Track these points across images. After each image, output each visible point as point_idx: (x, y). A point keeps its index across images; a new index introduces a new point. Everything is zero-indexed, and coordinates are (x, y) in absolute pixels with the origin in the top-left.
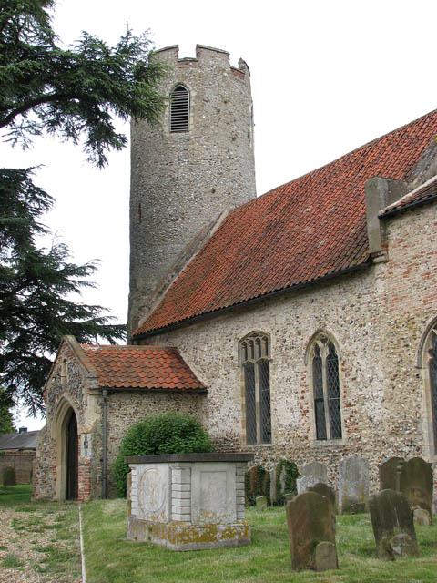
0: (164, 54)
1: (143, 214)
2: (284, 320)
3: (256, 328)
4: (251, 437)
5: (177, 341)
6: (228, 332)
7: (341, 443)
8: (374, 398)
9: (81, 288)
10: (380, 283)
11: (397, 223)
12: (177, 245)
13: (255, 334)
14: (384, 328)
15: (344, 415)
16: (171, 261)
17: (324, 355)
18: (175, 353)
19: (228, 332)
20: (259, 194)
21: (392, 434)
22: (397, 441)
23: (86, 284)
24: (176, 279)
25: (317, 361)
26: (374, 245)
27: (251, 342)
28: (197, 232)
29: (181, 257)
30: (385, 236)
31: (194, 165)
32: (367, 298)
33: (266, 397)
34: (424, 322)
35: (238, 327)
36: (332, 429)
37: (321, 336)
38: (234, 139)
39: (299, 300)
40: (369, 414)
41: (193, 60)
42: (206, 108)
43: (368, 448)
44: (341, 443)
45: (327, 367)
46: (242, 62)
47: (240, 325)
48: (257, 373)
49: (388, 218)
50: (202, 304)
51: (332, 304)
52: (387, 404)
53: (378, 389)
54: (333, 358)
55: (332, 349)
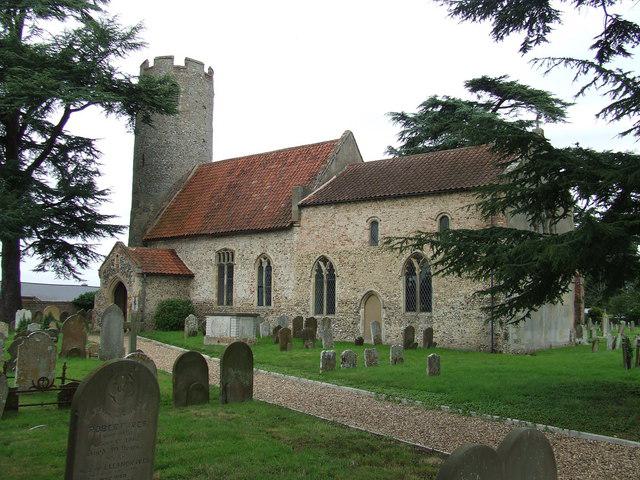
4: (260, 303)
5: (174, 246)
7: (270, 308)
10: (296, 236)
12: (168, 184)
13: (226, 249)
14: (295, 257)
15: (273, 295)
16: (163, 193)
17: (265, 265)
18: (173, 252)
20: (215, 159)
22: (298, 309)
25: (261, 268)
26: (294, 218)
30: (300, 214)
31: (180, 135)
32: (288, 242)
33: (230, 283)
37: (264, 256)
41: (183, 68)
44: (270, 308)
45: (265, 271)
46: (210, 69)
48: (226, 270)
49: (302, 207)
50: (193, 227)
53: (291, 285)
54: (269, 268)
55: (269, 263)
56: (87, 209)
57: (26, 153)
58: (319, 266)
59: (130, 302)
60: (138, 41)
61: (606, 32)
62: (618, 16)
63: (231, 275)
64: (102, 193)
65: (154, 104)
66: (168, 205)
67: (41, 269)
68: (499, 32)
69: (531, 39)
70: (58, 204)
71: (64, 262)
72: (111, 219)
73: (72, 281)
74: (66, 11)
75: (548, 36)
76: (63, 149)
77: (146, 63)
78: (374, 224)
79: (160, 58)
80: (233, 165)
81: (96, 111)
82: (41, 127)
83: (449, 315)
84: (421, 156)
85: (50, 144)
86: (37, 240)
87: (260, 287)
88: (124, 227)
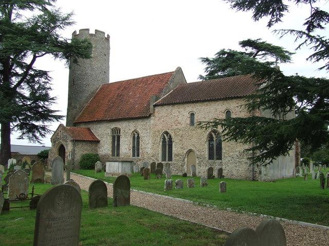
4: (134, 155)
5: (89, 126)
7: (139, 158)
10: (152, 121)
13: (116, 128)
14: (152, 132)
15: (140, 151)
16: (84, 99)
17: (136, 136)
18: (89, 129)
20: (110, 82)
25: (134, 137)
26: (151, 112)
29: (88, 98)
30: (154, 110)
31: (92, 69)
32: (148, 124)
33: (118, 145)
37: (135, 131)
44: (139, 158)
45: (136, 139)
46: (108, 35)
48: (116, 138)
49: (155, 106)
50: (99, 116)
53: (150, 146)
54: (138, 137)
55: (138, 135)
56: (45, 107)
57: (14, 79)
58: (164, 136)
59: (67, 154)
60: (71, 21)
61: (311, 16)
62: (317, 8)
63: (119, 141)
64: (52, 99)
65: (79, 54)
66: (86, 105)
67: (21, 138)
68: (256, 16)
69: (273, 20)
70: (30, 105)
71: (33, 134)
73: (37, 144)
74: (34, 6)
75: (282, 19)
76: (32, 76)
77: (75, 32)
78: (192, 115)
79: (82, 30)
80: (120, 85)
81: (49, 57)
82: (21, 65)
83: (231, 161)
84: (216, 80)
85: (26, 74)
86: (19, 123)
87: (134, 147)
88: (64, 116)
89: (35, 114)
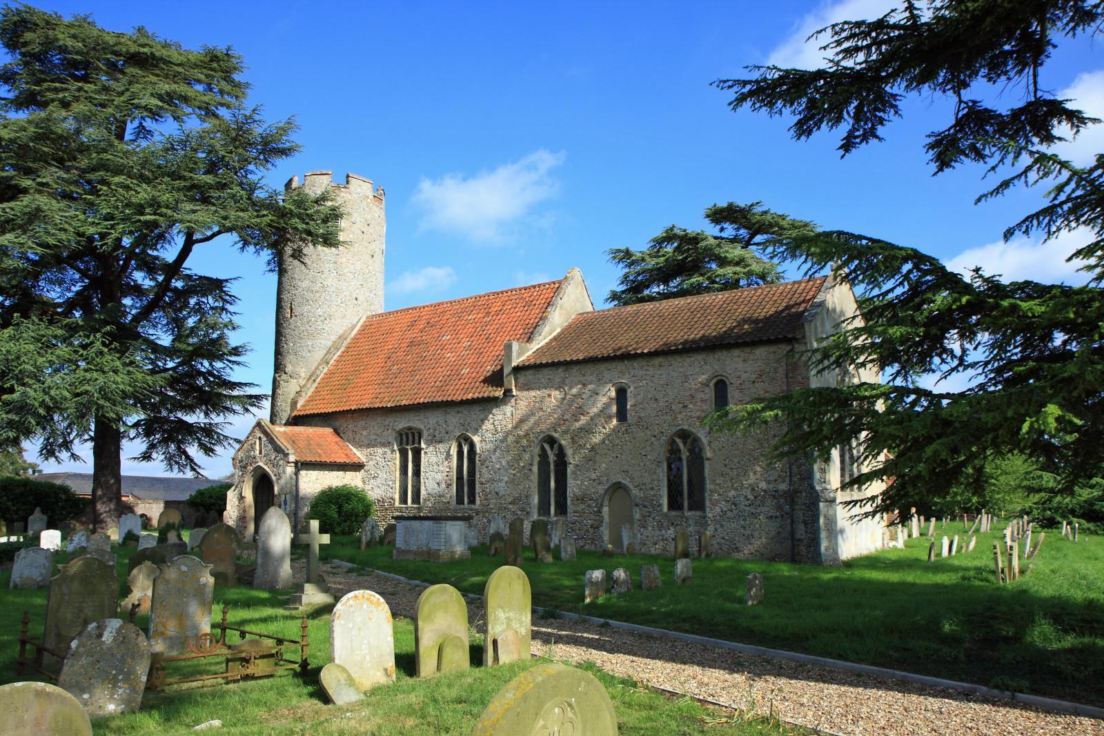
0: (320, 177)
1: (294, 311)
2: (435, 421)
3: (411, 424)
6: (387, 423)
8: (501, 481)
9: (235, 367)
11: (524, 373)
13: (410, 428)
16: (319, 355)
17: (552, 458)
19: (387, 423)
21: (510, 503)
23: (238, 363)
24: (325, 370)
27: (407, 435)
28: (341, 332)
34: (537, 438)
35: (395, 421)
36: (469, 498)
38: (373, 256)
39: (449, 410)
40: (496, 490)
42: (353, 229)
43: (494, 511)
47: (398, 420)
51: (474, 416)
52: (508, 485)
56: (213, 375)
57: (127, 301)
58: (543, 449)
61: (955, 126)
62: (974, 102)
64: (236, 351)
65: (309, 233)
67: (146, 457)
68: (803, 129)
69: (857, 133)
70: (173, 369)
71: (179, 448)
72: (247, 389)
73: (189, 474)
75: (880, 130)
78: (721, 388)
82: (150, 266)
83: (729, 514)
84: (648, 306)
85: (164, 287)
86: (143, 417)
89: (185, 394)
